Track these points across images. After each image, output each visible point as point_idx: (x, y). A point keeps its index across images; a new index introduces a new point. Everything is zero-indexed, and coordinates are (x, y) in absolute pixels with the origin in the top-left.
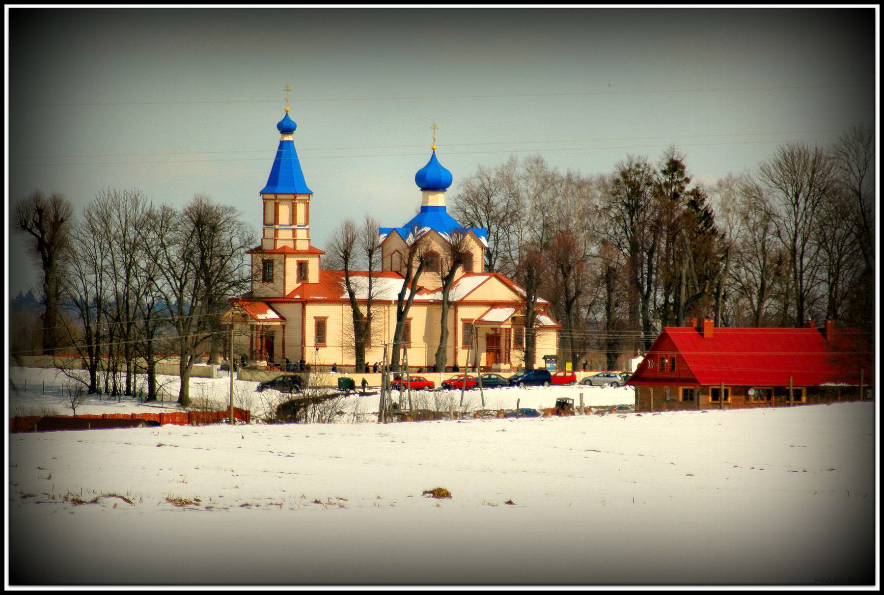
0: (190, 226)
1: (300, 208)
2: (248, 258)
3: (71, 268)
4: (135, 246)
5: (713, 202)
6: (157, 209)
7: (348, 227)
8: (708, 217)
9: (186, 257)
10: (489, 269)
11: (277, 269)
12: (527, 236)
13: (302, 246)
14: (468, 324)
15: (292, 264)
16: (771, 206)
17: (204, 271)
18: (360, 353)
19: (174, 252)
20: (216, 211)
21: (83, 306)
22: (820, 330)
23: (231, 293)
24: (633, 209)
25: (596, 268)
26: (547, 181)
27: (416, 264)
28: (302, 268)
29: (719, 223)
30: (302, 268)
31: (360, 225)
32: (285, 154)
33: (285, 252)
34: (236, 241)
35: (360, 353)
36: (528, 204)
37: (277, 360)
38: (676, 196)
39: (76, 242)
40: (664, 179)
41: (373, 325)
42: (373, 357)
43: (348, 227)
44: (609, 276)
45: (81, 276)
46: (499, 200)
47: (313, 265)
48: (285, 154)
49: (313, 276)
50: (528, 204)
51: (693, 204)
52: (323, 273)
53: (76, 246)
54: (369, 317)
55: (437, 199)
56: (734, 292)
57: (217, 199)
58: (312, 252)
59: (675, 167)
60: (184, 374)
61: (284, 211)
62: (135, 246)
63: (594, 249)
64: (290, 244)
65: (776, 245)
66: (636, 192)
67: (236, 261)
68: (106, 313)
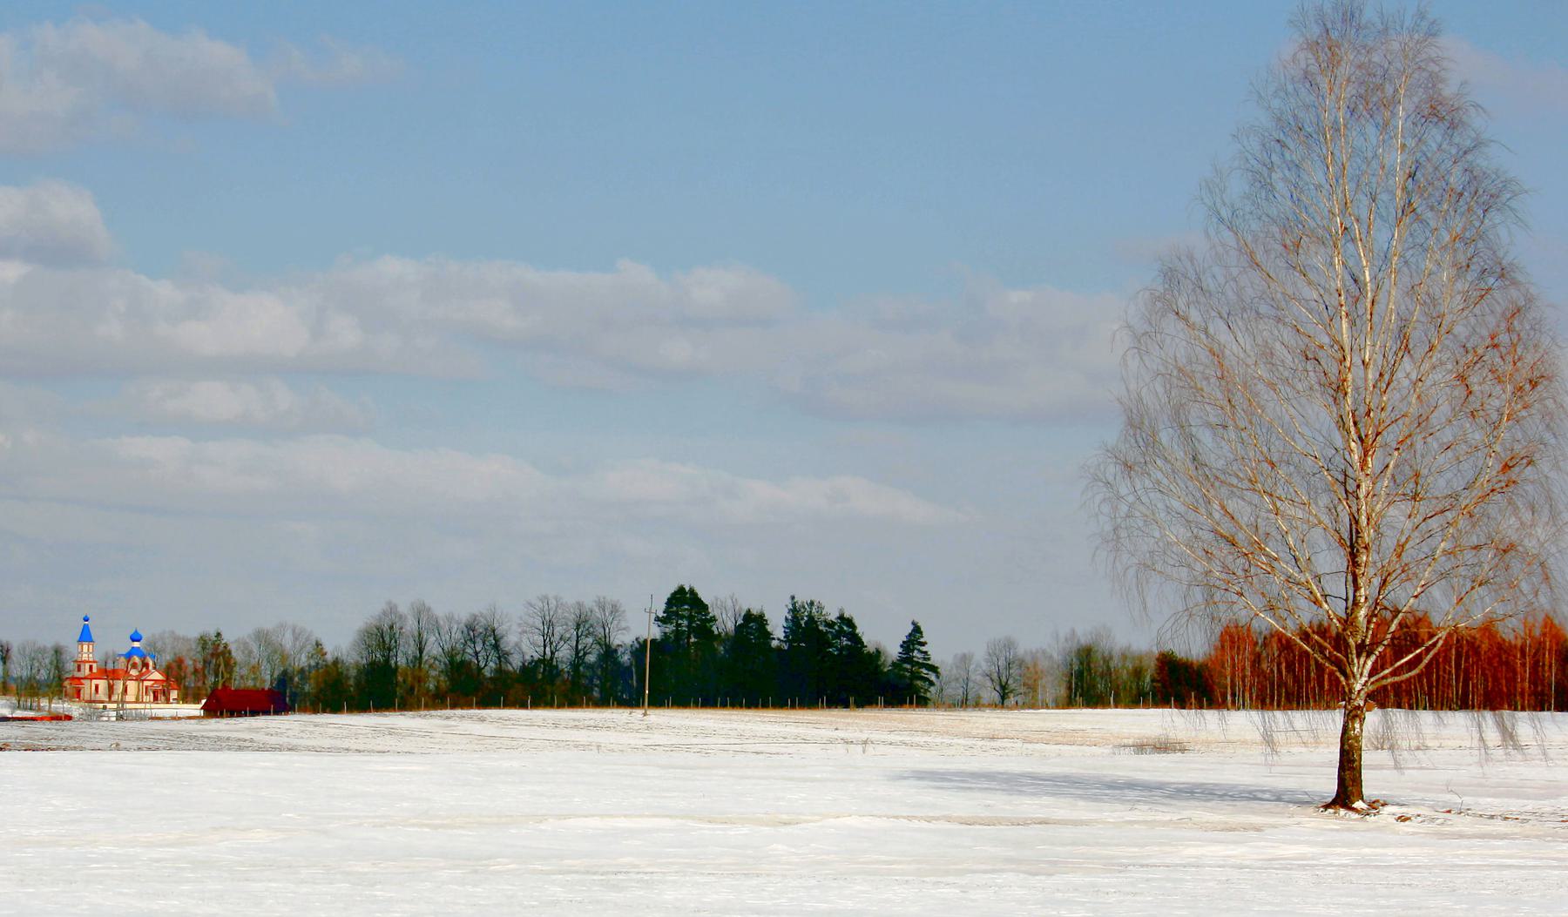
0: (53, 652)
1: (91, 646)
2: (72, 664)
3: (12, 666)
4: (34, 659)
5: (233, 647)
6: (42, 647)
7: (107, 654)
8: (230, 652)
9: (51, 663)
10: (155, 668)
11: (82, 667)
12: (168, 658)
13: (91, 660)
14: (147, 688)
15: (87, 666)
16: (1560, 623)
17: (57, 668)
18: (110, 697)
19: (47, 661)
20: (557, 666)
21: (15, 680)
22: (90, 640)
23: (67, 676)
24: (204, 649)
25: (191, 669)
26: (177, 639)
27: (130, 667)
28: (91, 667)
29: (234, 654)
30: (91, 667)
31: (111, 653)
32: (86, 628)
33: (85, 662)
34: (68, 658)
35: (110, 697)
36: (169, 647)
37: (81, 698)
38: (219, 645)
39: (1493, 509)
40: (215, 639)
41: (115, 687)
42: (115, 698)
43: (107, 654)
44: (196, 671)
45: (15, 668)
46: (159, 645)
47: (95, 665)
48: (86, 628)
49: (95, 670)
50: (169, 647)
51: (225, 647)
52: (98, 669)
53: (14, 659)
54: (113, 685)
55: (136, 644)
56: (238, 678)
57: (63, 643)
58: (94, 662)
59: (219, 635)
60: (50, 702)
61: (85, 647)
62: (34, 659)
63: (191, 663)
64: (87, 659)
65: (254, 662)
66: (205, 643)
67: (68, 664)
68: (1318, 238)
